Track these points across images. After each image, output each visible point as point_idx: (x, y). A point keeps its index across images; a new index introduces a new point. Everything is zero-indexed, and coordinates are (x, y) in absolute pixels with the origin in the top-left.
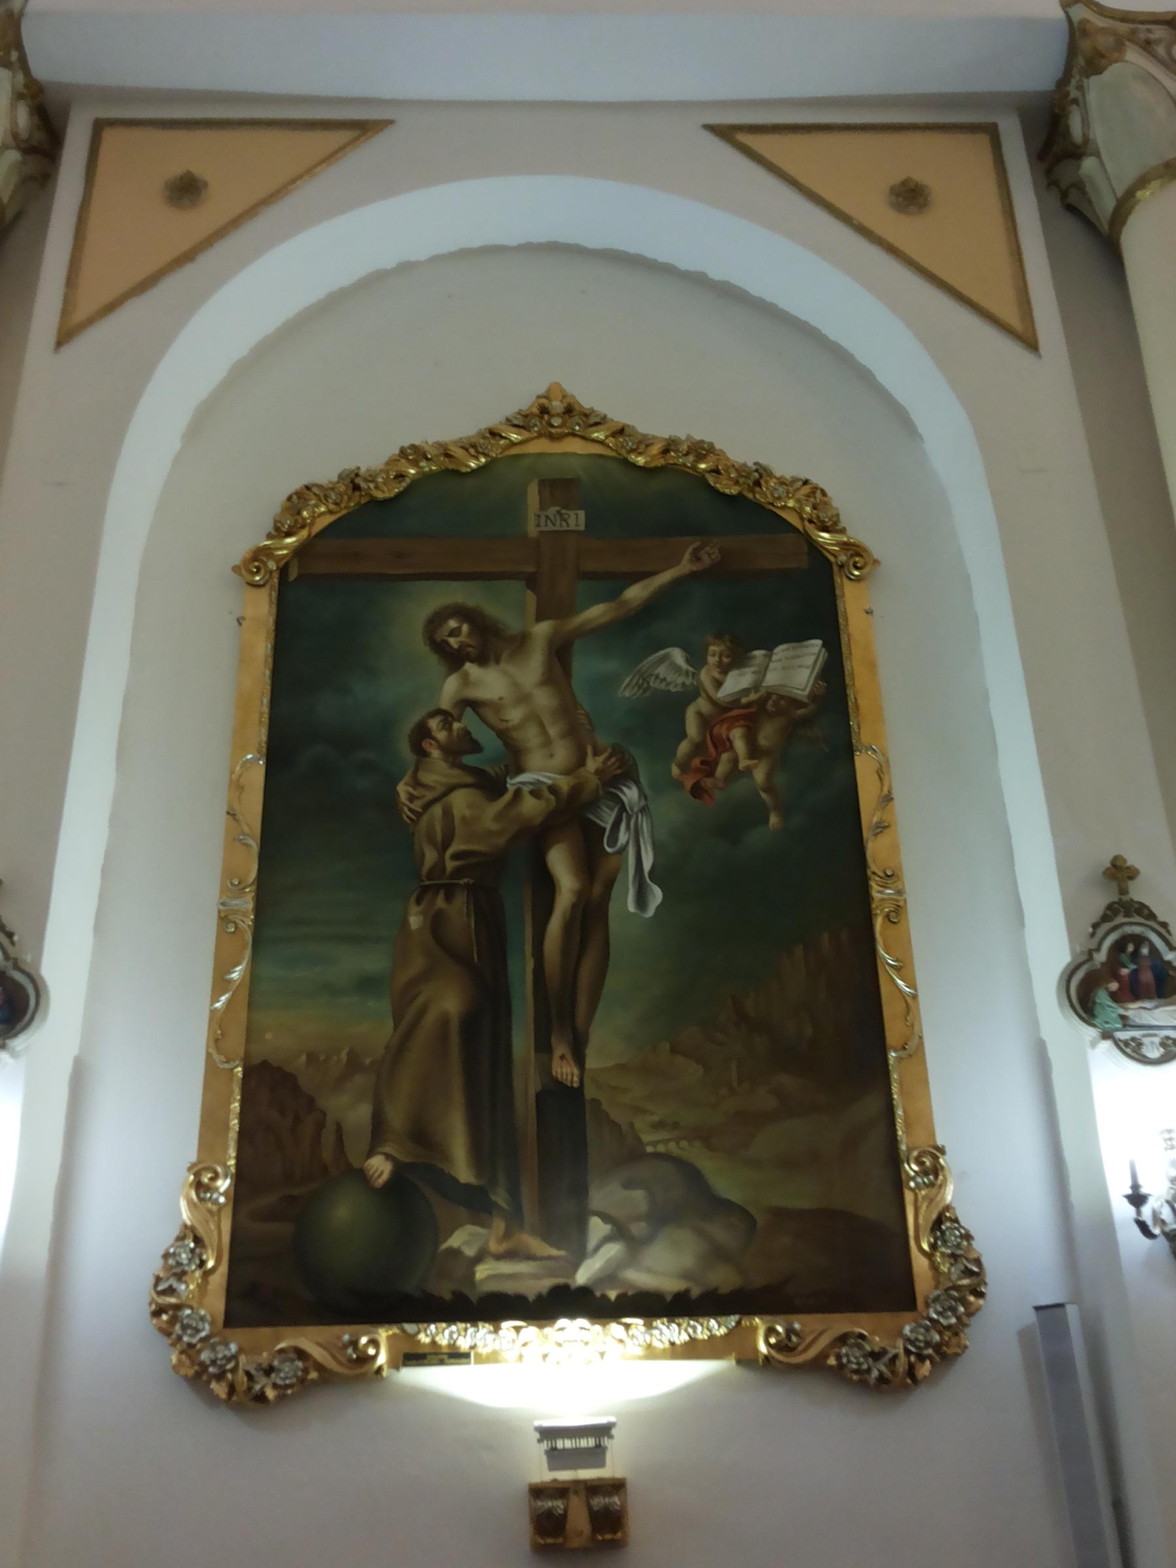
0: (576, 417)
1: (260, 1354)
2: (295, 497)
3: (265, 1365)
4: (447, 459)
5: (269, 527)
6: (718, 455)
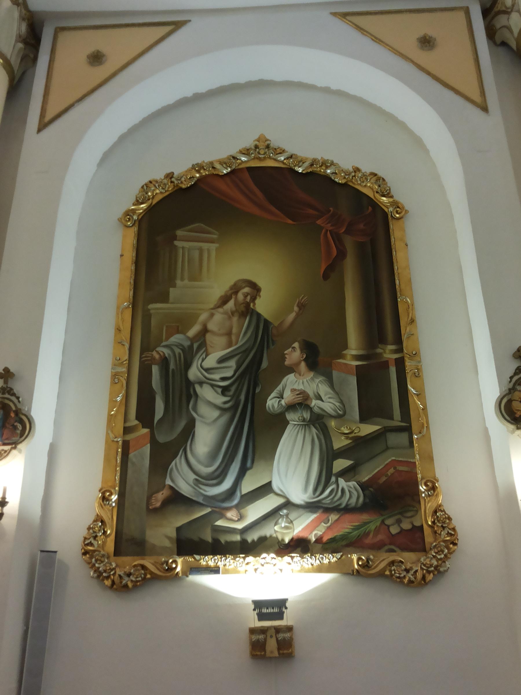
0: (271, 150)
1: (125, 567)
2: (145, 186)
3: (127, 572)
4: (213, 169)
5: (134, 200)
6: (335, 166)
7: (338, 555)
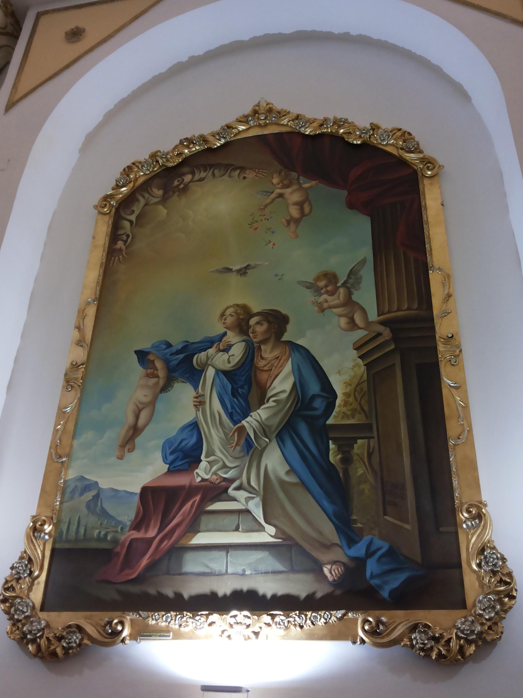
7: (339, 614)
